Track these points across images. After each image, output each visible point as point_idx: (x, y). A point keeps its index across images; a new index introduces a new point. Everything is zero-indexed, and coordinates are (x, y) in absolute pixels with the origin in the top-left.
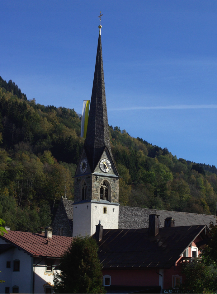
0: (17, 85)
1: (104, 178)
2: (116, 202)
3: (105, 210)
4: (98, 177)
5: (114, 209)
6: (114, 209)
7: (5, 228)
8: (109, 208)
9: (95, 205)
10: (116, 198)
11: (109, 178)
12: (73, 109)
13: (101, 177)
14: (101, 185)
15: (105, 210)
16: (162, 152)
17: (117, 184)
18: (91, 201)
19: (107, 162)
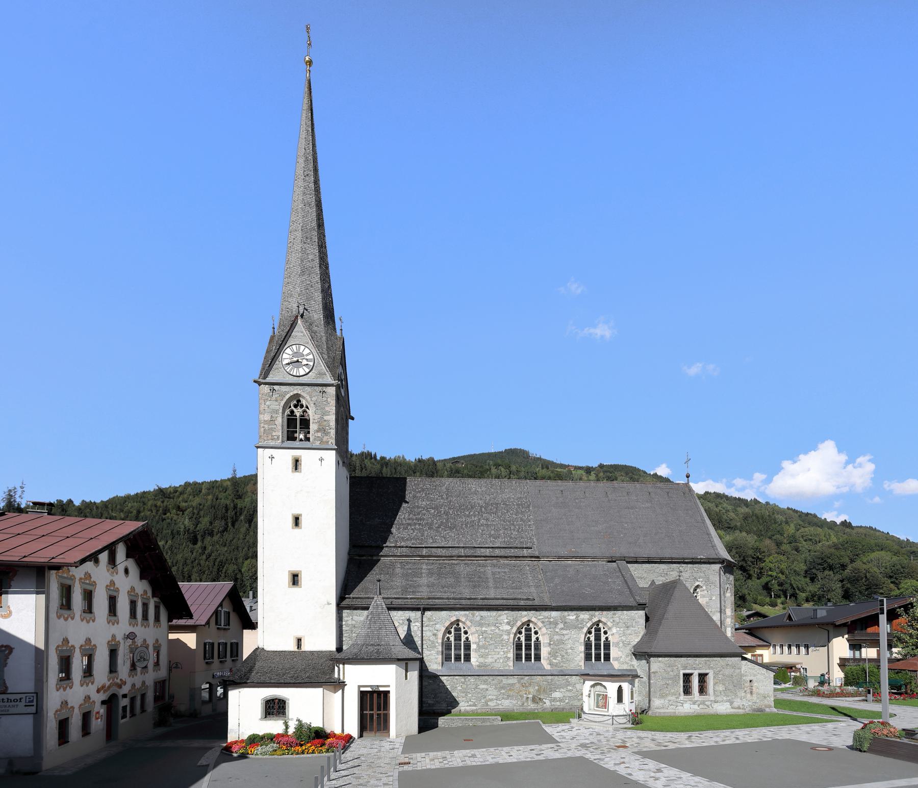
0: (158, 486)
1: (291, 388)
2: (817, 599)
3: (297, 463)
4: (276, 387)
5: (321, 460)
6: (321, 460)
7: (34, 644)
8: (308, 457)
9: (269, 452)
10: (327, 434)
11: (307, 388)
12: (83, 501)
13: (284, 388)
14: (307, 407)
15: (297, 463)
16: (569, 284)
17: (329, 400)
18: (761, 662)
19: (301, 351)
